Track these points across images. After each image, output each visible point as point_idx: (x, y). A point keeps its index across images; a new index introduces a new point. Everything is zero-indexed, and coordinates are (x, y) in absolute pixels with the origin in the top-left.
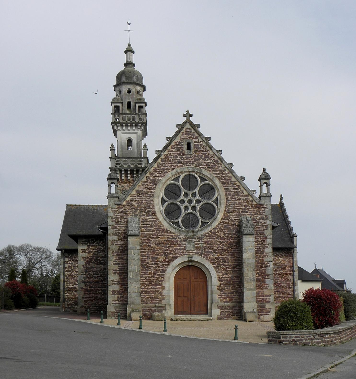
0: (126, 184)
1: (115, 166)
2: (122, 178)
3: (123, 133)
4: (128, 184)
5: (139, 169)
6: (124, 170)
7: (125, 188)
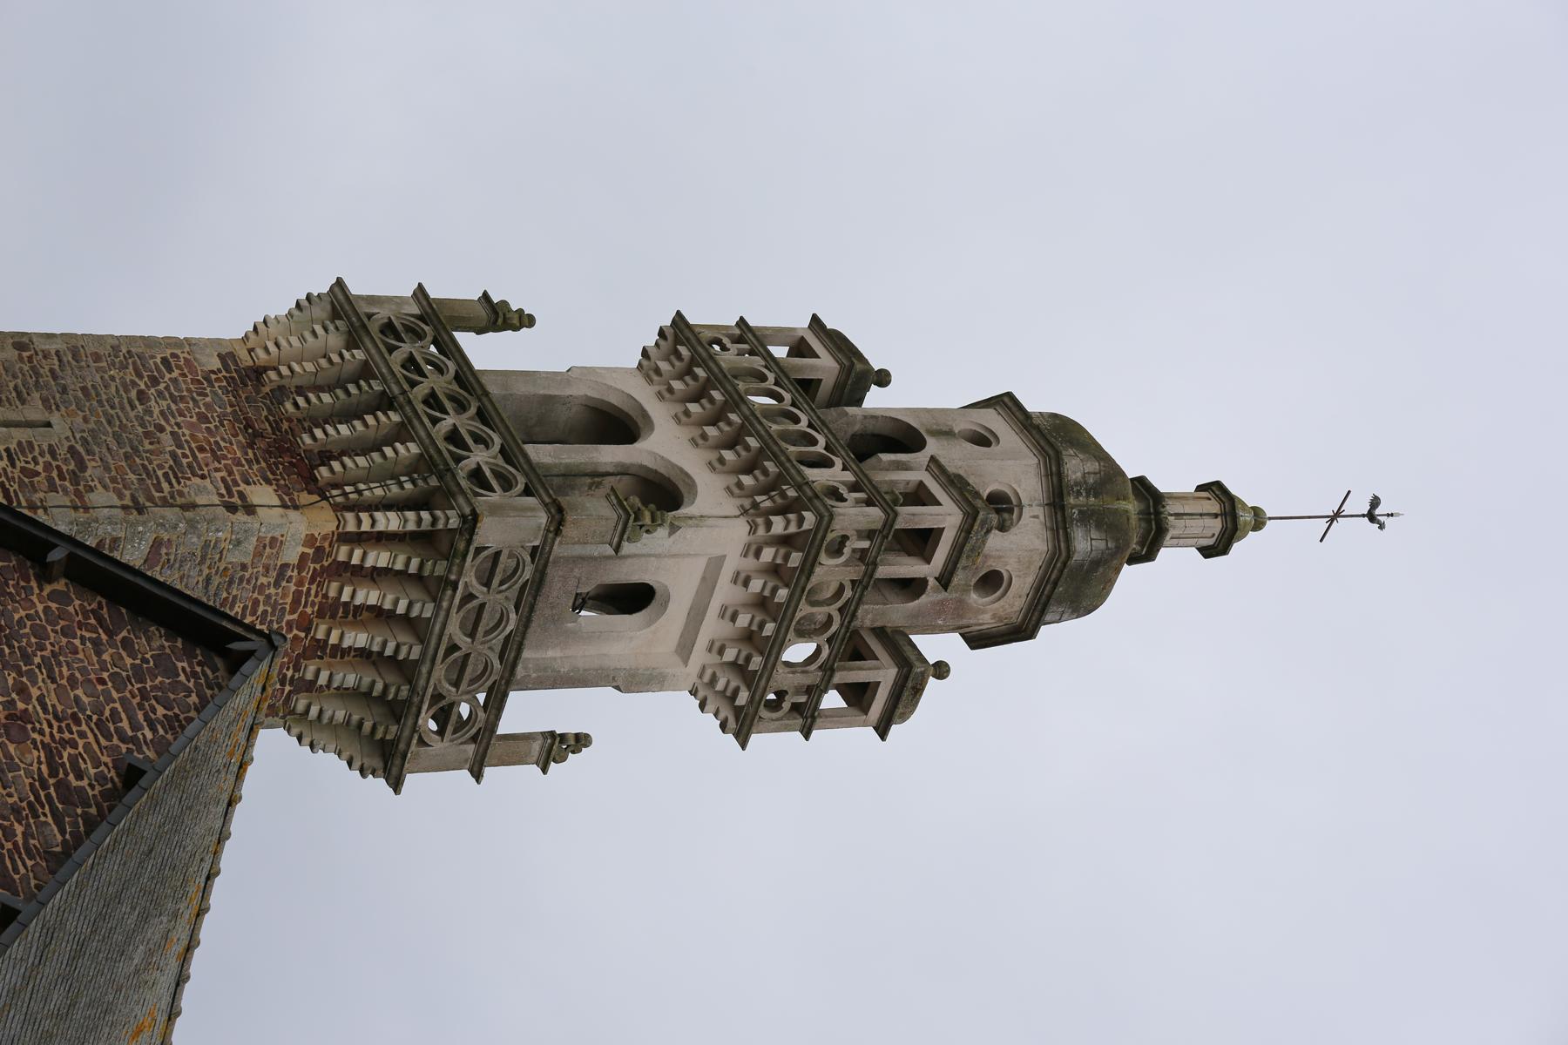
0: (296, 602)
1: (479, 550)
2: (381, 654)
3: (716, 564)
4: (288, 617)
5: (398, 722)
6: (427, 614)
7: (261, 598)
